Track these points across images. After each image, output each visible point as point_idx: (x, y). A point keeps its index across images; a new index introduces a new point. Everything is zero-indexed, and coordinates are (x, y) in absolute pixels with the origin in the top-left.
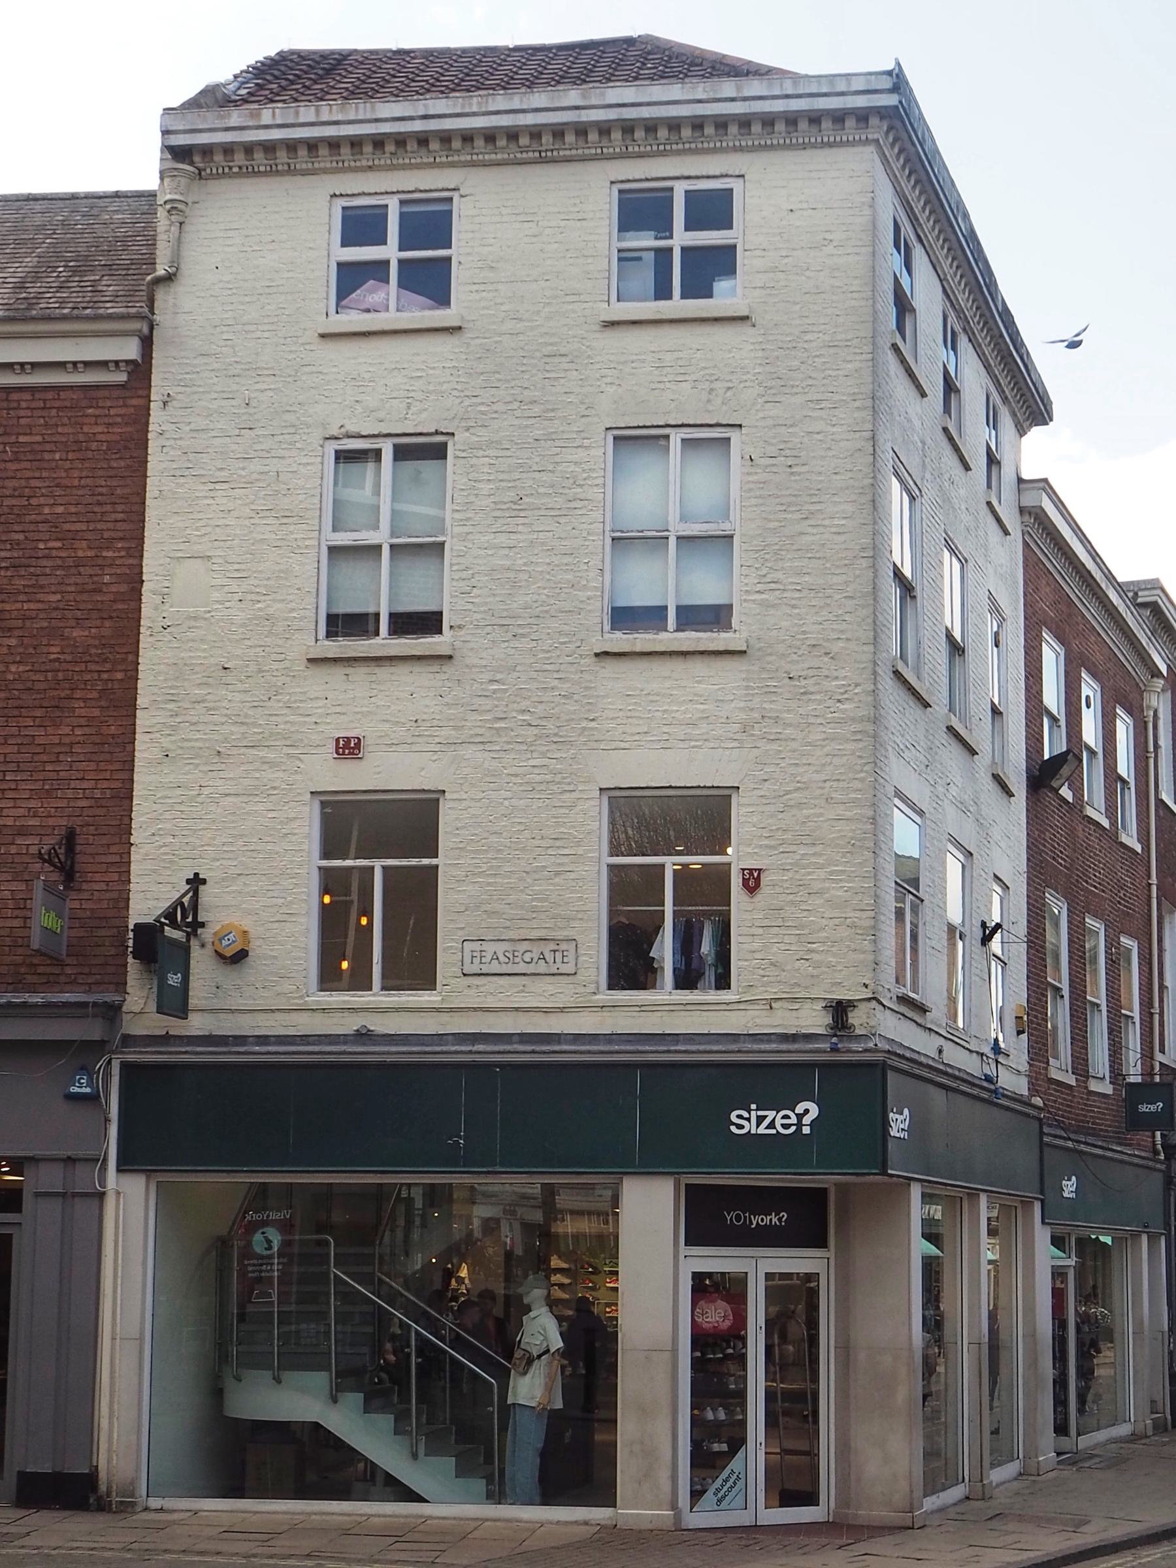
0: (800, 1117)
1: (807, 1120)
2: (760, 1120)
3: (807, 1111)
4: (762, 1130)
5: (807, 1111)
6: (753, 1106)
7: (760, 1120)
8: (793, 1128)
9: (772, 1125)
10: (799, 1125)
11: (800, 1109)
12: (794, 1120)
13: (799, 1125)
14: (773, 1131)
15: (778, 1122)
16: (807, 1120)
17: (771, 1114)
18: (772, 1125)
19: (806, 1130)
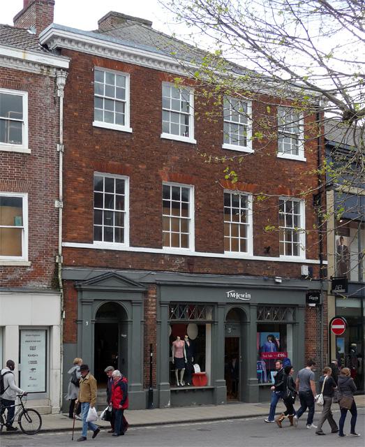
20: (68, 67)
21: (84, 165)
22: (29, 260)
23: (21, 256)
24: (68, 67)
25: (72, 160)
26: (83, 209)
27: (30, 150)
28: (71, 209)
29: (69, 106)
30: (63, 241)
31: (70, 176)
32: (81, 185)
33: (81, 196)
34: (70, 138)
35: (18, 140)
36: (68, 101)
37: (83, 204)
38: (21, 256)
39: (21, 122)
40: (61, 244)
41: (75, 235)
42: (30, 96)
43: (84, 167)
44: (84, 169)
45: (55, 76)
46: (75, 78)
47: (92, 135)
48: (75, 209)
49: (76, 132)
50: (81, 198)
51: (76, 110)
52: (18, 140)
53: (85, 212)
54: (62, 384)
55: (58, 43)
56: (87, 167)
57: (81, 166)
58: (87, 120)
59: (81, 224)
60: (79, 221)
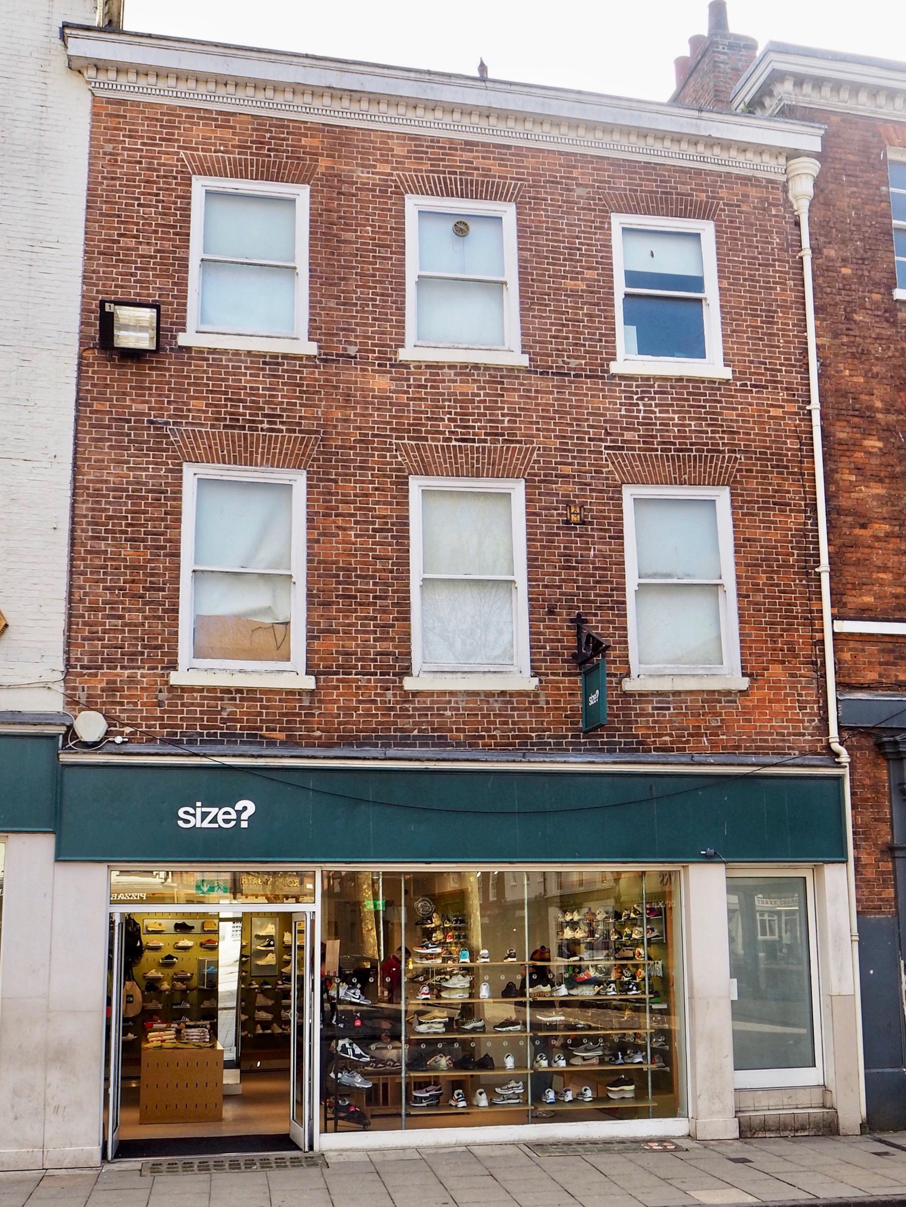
0: (239, 813)
1: (245, 816)
2: (204, 815)
3: (245, 808)
4: (206, 824)
5: (245, 808)
6: (199, 804)
7: (204, 815)
8: (233, 823)
9: (214, 820)
10: (238, 820)
11: (239, 806)
12: (234, 816)
13: (238, 820)
14: (216, 826)
15: (220, 817)
16: (245, 816)
17: (214, 811)
18: (214, 820)
19: (244, 825)
20: (819, 149)
21: (879, 404)
22: (744, 675)
23: (704, 357)
24: (819, 149)
25: (845, 395)
26: (887, 527)
27: (730, 369)
28: (852, 527)
29: (825, 251)
30: (834, 618)
31: (843, 435)
32: (874, 461)
33: (878, 490)
34: (836, 335)
35: (696, 349)
36: (822, 239)
37: (884, 511)
38: (704, 357)
39: (700, 300)
40: (830, 627)
41: (869, 599)
42: (619, 211)
43: (878, 410)
44: (879, 416)
45: (783, 178)
46: (836, 179)
47: (894, 324)
48: (864, 526)
49: (848, 319)
50: (877, 497)
51: (844, 260)
52: (696, 349)
53: (888, 535)
54: (884, 1199)
55: (785, 90)
56: (887, 411)
57: (870, 408)
58: (876, 284)
59: (885, 569)
60: (877, 559)
